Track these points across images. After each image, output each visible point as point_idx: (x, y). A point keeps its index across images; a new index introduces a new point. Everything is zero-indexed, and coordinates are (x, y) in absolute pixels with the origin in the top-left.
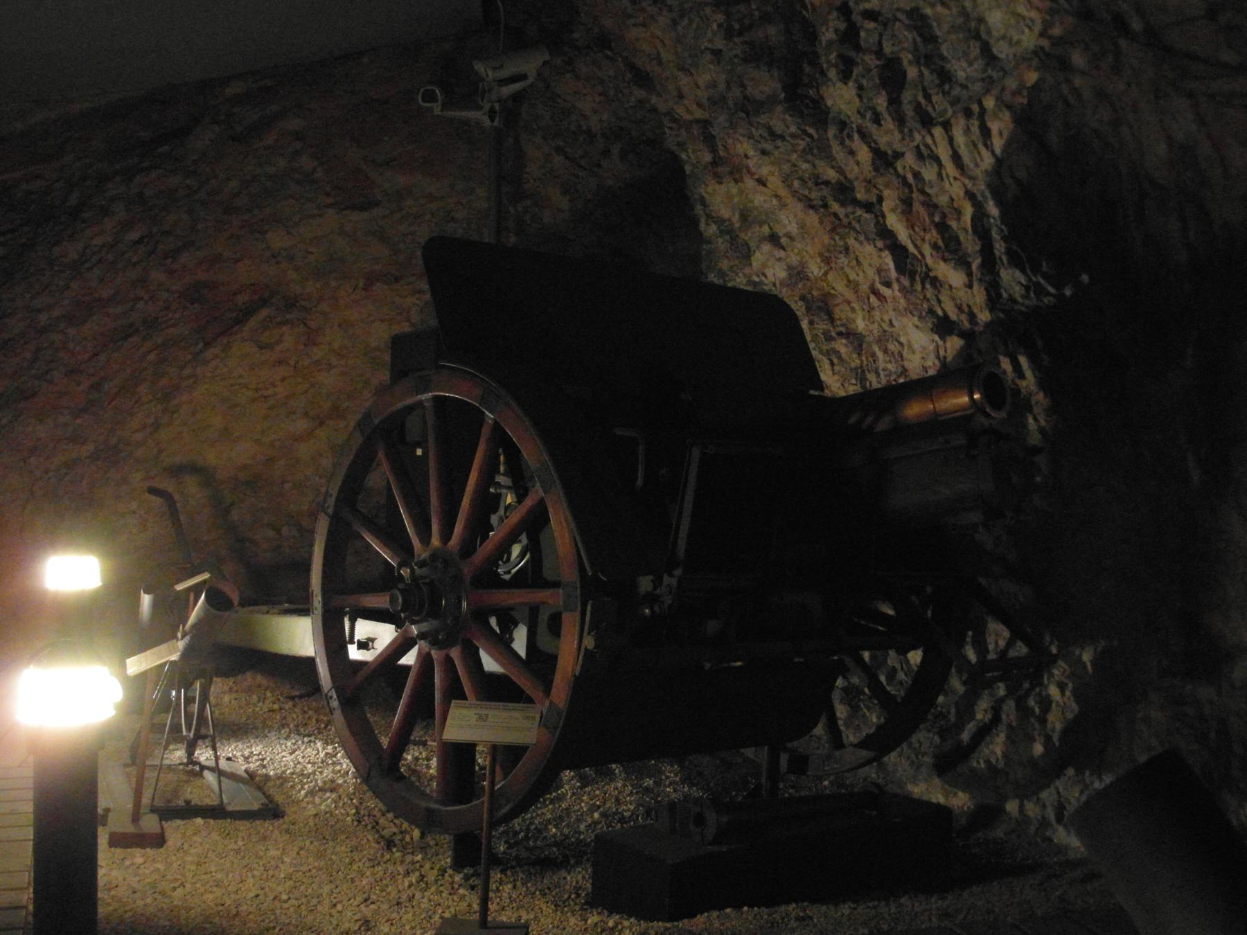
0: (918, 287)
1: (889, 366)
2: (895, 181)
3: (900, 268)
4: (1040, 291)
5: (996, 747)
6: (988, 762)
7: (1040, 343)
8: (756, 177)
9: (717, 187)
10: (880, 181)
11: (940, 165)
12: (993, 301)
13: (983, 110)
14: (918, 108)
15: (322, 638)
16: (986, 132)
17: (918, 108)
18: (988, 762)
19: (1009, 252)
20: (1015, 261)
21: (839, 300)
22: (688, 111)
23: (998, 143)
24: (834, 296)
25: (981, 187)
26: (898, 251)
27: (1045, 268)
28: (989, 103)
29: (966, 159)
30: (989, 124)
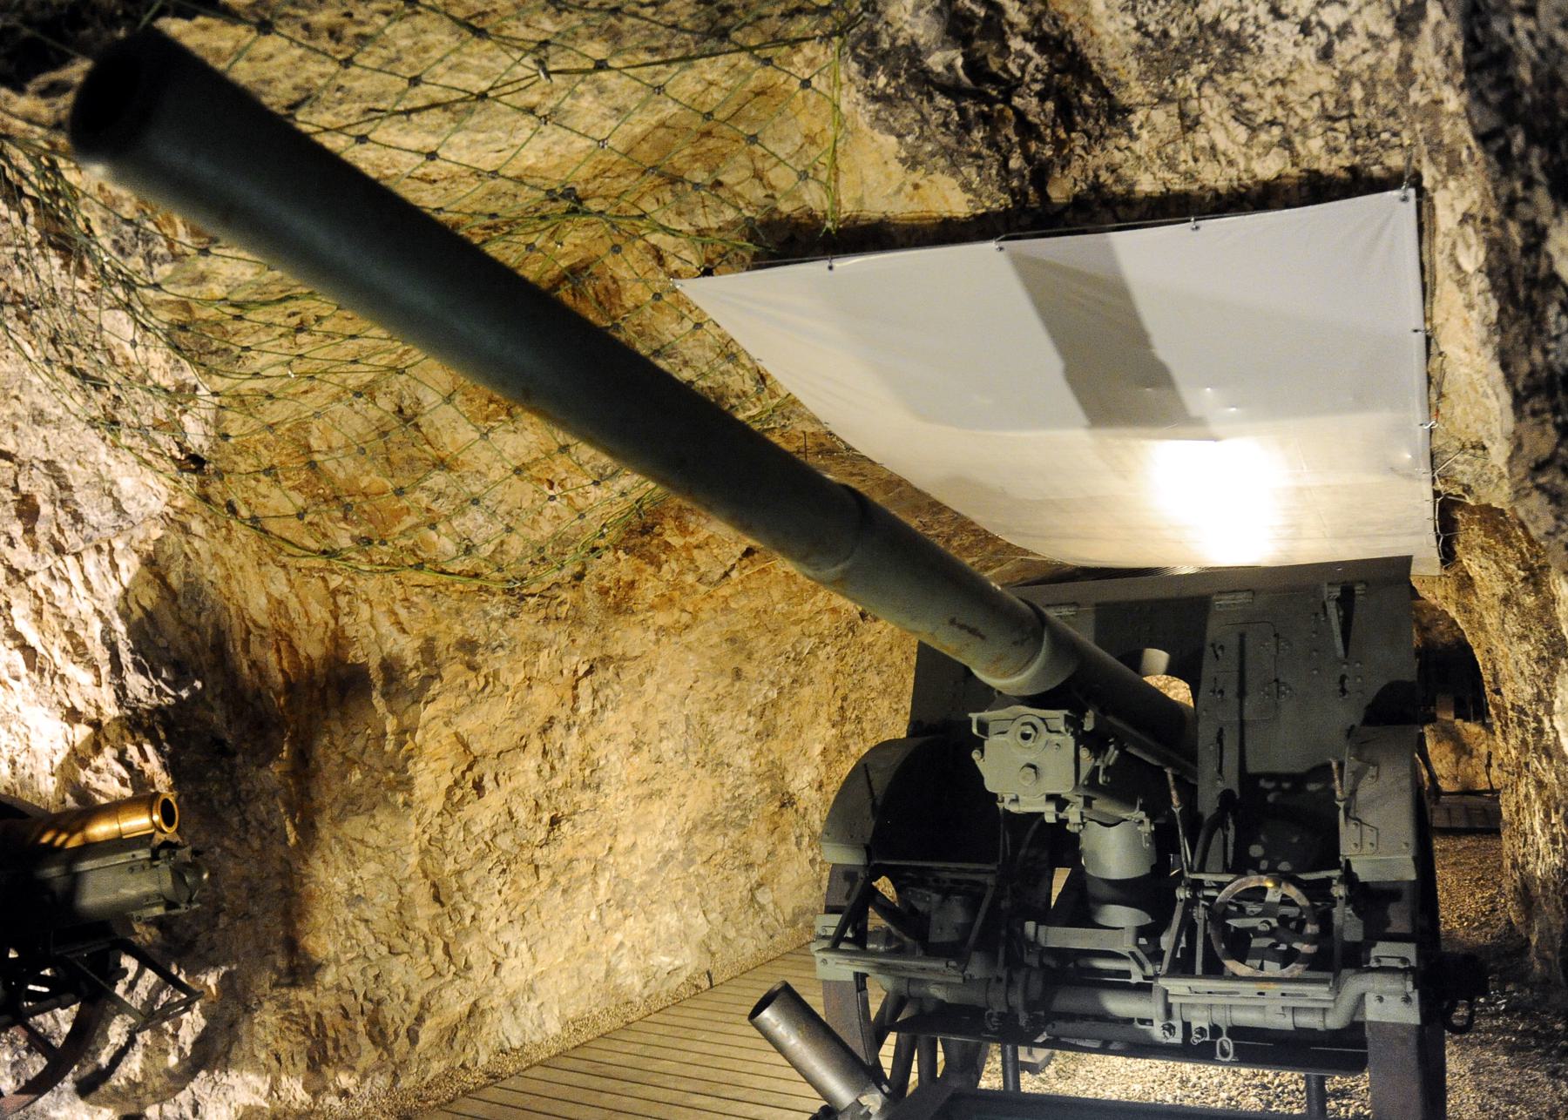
0: (48, 682)
1: (13, 744)
2: (27, 594)
3: (30, 665)
4: (160, 692)
5: (133, 1066)
6: (128, 1079)
7: (162, 735)
10: (12, 593)
11: (71, 585)
12: (121, 699)
13: (112, 550)
14: (52, 539)
16: (114, 566)
17: (52, 539)
18: (128, 1079)
19: (135, 662)
20: (140, 669)
23: (126, 578)
25: (109, 608)
26: (28, 651)
27: (164, 674)
28: (119, 544)
29: (96, 584)
30: (117, 561)
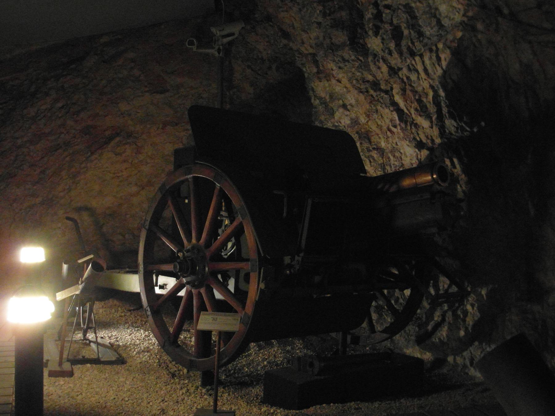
8: (337, 79)
9: (319, 83)
15: (143, 284)
21: (373, 134)
22: (306, 49)
24: (371, 132)
